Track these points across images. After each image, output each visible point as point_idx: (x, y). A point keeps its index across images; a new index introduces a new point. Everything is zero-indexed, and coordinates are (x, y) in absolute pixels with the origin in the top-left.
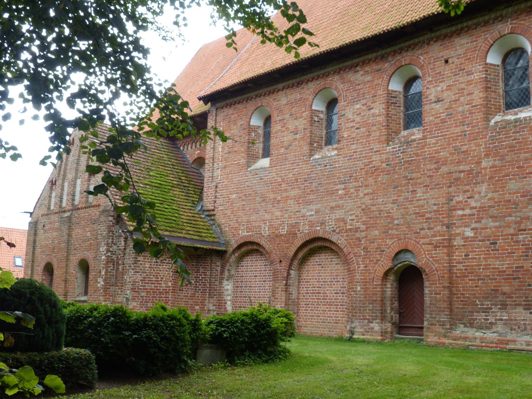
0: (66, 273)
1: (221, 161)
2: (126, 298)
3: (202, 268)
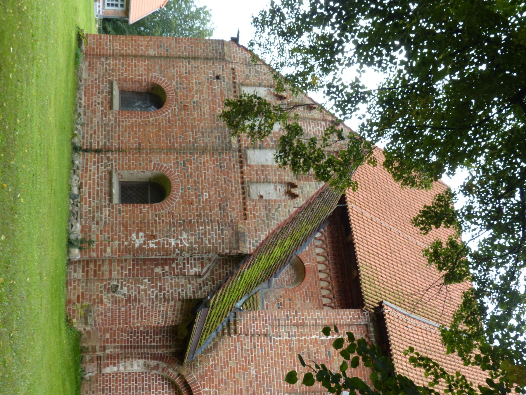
0: (152, 150)
1: (299, 340)
2: (117, 286)
3: (160, 338)
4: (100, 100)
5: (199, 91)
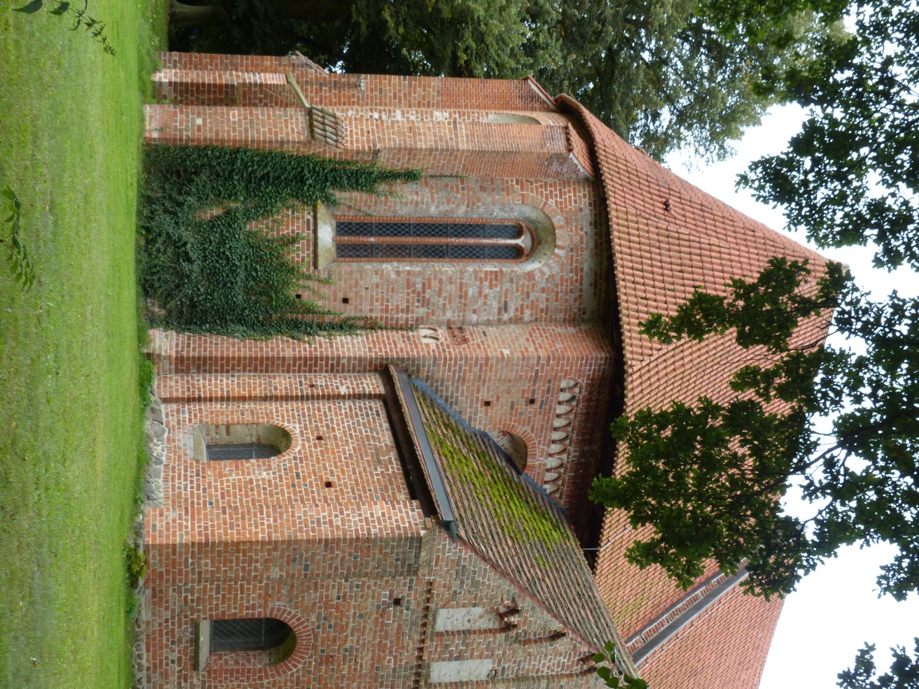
4: (175, 656)
5: (359, 630)
